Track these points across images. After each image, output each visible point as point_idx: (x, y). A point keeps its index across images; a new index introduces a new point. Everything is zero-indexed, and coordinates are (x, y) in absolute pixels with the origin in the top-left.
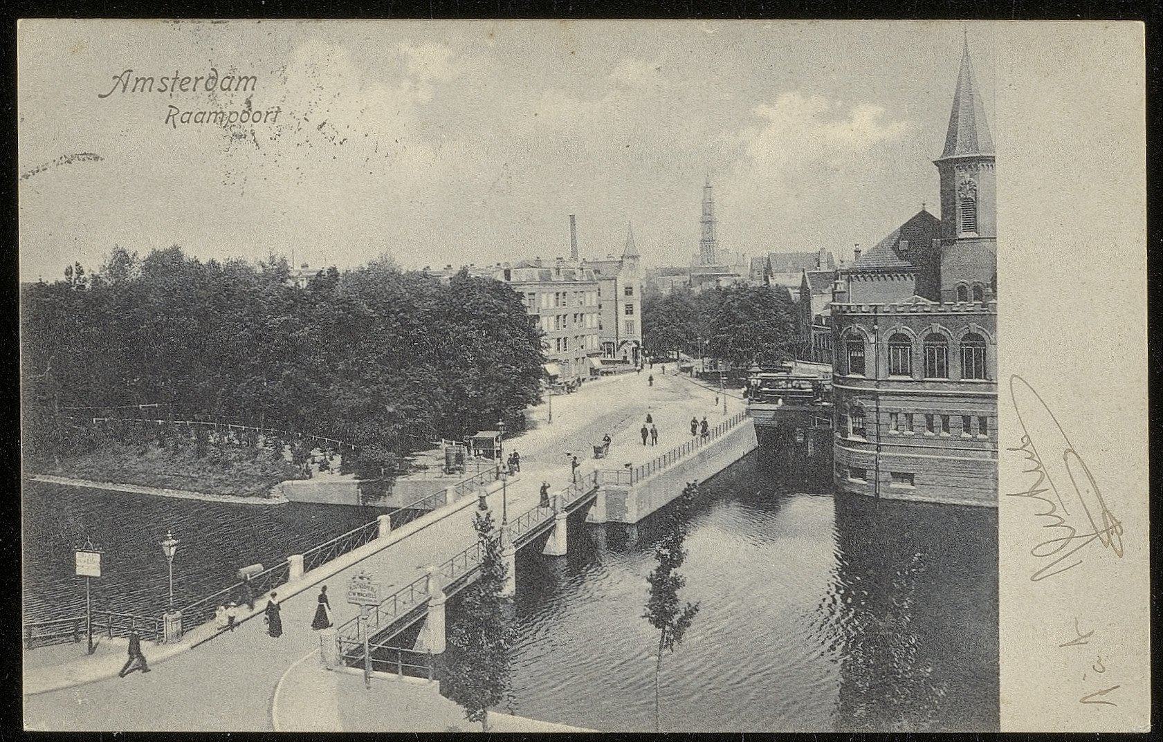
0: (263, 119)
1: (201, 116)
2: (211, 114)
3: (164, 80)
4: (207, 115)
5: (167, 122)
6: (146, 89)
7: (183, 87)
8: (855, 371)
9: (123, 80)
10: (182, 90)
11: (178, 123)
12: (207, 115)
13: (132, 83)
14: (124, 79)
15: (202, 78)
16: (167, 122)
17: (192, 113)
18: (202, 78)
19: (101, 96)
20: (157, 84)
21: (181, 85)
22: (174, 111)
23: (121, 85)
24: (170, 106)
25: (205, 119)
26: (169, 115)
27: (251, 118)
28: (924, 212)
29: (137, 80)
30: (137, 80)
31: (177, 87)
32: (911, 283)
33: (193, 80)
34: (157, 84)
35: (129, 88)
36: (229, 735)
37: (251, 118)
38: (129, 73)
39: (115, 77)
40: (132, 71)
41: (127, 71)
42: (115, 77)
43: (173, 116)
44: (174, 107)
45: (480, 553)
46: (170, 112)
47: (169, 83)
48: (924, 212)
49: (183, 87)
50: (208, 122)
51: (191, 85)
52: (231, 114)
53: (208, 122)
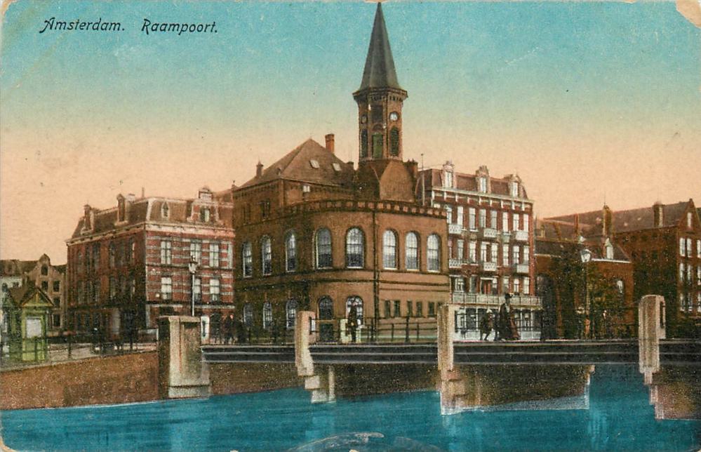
0: (204, 30)
2: (112, 24)
4: (168, 26)
5: (143, 30)
6: (116, 29)
11: (149, 30)
12: (168, 26)
13: (55, 24)
14: (51, 22)
16: (143, 30)
19: (41, 32)
20: (68, 25)
22: (147, 23)
24: (145, 20)
25: (108, 28)
32: (380, 287)
33: (87, 25)
34: (68, 25)
42: (46, 21)
47: (74, 26)
50: (110, 29)
51: (85, 28)
52: (97, 29)
53: (110, 29)
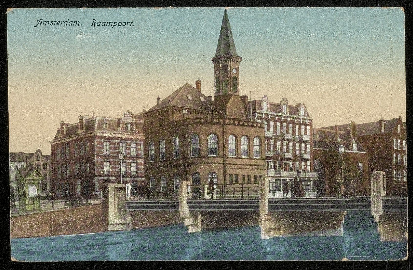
1: (104, 23)
3: (52, 22)
5: (92, 25)
7: (58, 24)
8: (298, 113)
9: (40, 22)
10: (57, 25)
11: (96, 26)
15: (63, 22)
16: (92, 25)
17: (101, 22)
18: (63, 22)
20: (50, 23)
21: (57, 23)
23: (40, 24)
24: (93, 20)
26: (93, 23)
27: (122, 24)
28: (187, 84)
29: (44, 22)
30: (44, 22)
31: (56, 24)
33: (61, 22)
34: (50, 23)
35: (42, 24)
36: (7, 127)
37: (122, 24)
38: (41, 20)
39: (38, 21)
40: (42, 19)
41: (41, 19)
42: (38, 21)
43: (94, 23)
44: (95, 20)
45: (129, 121)
46: (93, 22)
47: (54, 23)
48: (187, 84)
49: (58, 24)
53: (107, 25)
